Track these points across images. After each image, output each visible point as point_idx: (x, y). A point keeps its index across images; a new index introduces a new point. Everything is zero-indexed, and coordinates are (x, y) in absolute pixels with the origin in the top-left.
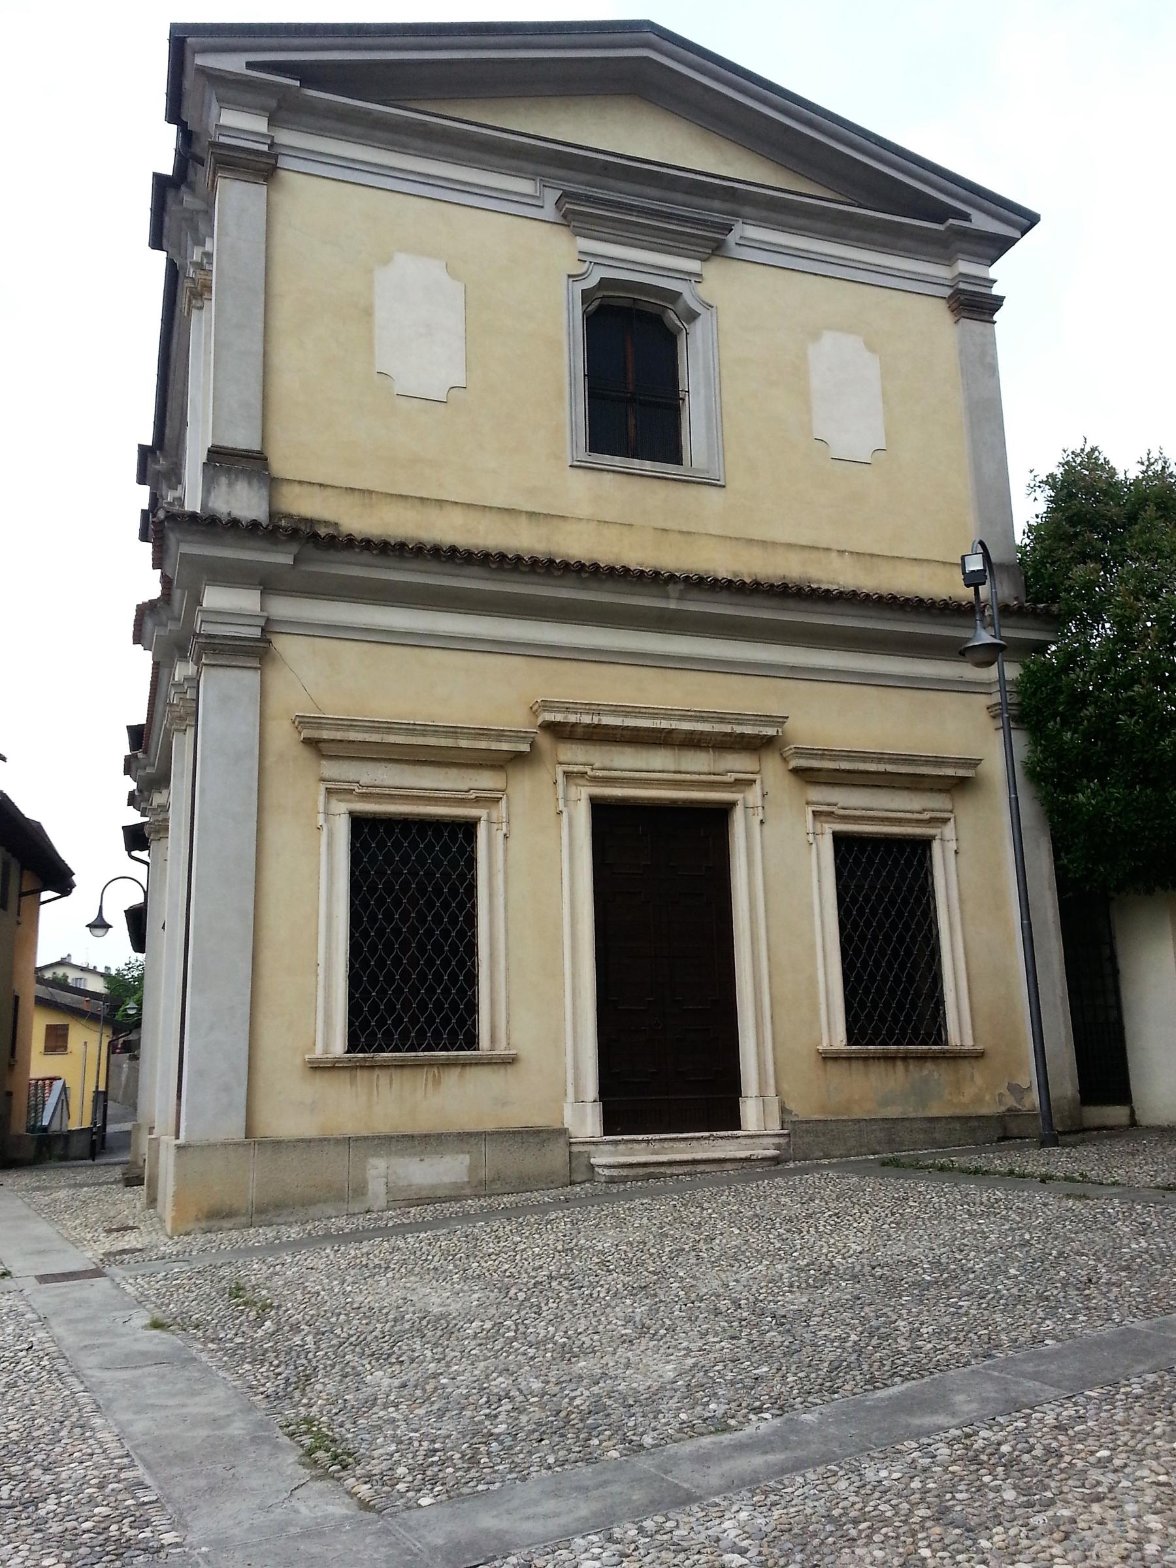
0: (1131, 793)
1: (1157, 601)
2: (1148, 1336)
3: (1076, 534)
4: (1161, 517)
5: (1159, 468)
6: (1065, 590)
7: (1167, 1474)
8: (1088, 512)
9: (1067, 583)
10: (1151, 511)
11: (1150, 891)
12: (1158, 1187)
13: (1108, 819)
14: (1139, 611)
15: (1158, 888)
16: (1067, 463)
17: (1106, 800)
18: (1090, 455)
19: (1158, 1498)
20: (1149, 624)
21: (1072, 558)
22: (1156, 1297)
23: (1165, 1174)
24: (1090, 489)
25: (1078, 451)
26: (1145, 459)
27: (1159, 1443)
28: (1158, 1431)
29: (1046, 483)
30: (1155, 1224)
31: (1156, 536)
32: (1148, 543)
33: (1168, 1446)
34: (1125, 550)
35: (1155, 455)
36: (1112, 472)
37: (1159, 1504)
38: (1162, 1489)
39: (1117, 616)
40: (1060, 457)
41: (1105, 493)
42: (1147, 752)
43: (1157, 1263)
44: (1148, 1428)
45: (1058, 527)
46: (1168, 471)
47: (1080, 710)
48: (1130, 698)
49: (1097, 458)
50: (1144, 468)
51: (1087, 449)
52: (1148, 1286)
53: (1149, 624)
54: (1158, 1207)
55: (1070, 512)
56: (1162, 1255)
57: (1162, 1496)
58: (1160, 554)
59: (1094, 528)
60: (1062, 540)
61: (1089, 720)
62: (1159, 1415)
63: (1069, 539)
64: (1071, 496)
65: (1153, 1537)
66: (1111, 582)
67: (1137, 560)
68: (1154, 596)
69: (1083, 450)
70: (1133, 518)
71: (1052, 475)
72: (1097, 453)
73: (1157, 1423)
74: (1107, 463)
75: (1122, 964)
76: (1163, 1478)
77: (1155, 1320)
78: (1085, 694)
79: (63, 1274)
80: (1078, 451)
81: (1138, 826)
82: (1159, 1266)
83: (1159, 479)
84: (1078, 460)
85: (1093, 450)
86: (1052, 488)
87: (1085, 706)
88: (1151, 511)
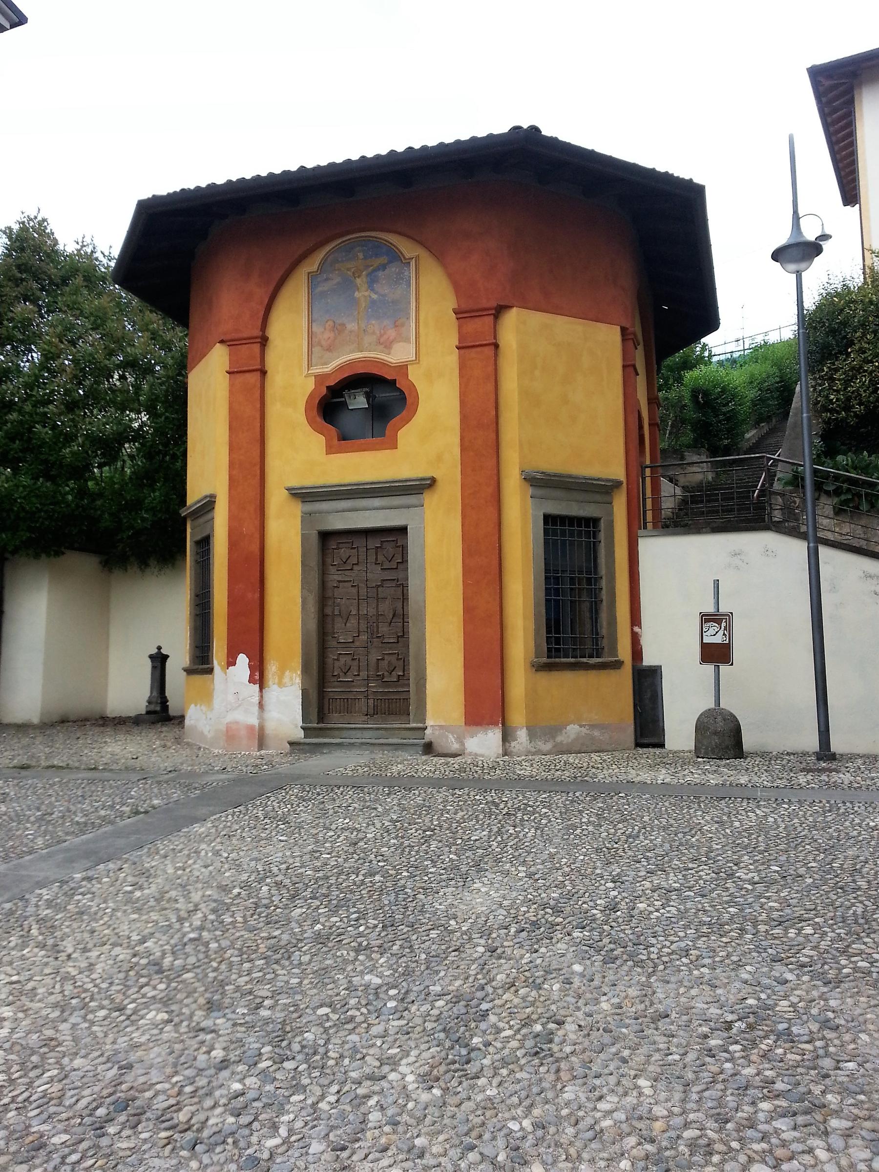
0: (35, 483)
1: (75, 347)
2: (6, 875)
3: (22, 280)
4: (86, 286)
5: (89, 251)
6: (7, 320)
7: (18, 974)
8: (33, 265)
9: (11, 315)
10: (79, 280)
11: (37, 556)
12: (15, 767)
13: (15, 500)
14: (61, 352)
15: (43, 556)
16: (23, 223)
17: (16, 485)
18: (40, 223)
19: (11, 994)
20: (66, 362)
21: (16, 296)
22: (12, 847)
23: (19, 758)
24: (37, 249)
25: (33, 217)
26: (80, 241)
27: (13, 953)
28: (12, 944)
29: (5, 233)
30: (12, 793)
31: (80, 299)
32: (75, 303)
33: (19, 954)
34: (56, 303)
35: (88, 240)
36: (56, 242)
37: (11, 998)
38: (14, 986)
39: (44, 350)
40: (19, 217)
41: (48, 256)
42: (52, 455)
43: (14, 821)
44: (5, 943)
45: (9, 269)
46: (95, 255)
47: (6, 414)
48: (45, 414)
49: (46, 227)
50: (79, 247)
51: (39, 218)
52: (7, 838)
53: (66, 362)
54: (16, 781)
55: (19, 262)
56: (17, 815)
57: (14, 991)
58: (82, 314)
59: (37, 279)
60: (10, 280)
61: (12, 423)
62: (13, 932)
63: (18, 282)
64: (22, 249)
65: (6, 1023)
66: (47, 324)
67: (65, 312)
68: (73, 343)
69: (36, 218)
70: (65, 281)
71: (10, 228)
72: (46, 224)
73: (11, 939)
74: (53, 234)
75: (7, 607)
76: (15, 978)
77: (11, 864)
78: (12, 403)
79: (802, 292)
80: (33, 217)
81: (37, 508)
82: (14, 824)
83: (88, 259)
84: (32, 224)
85: (44, 220)
86: (10, 238)
87: (9, 412)
88: (79, 280)
